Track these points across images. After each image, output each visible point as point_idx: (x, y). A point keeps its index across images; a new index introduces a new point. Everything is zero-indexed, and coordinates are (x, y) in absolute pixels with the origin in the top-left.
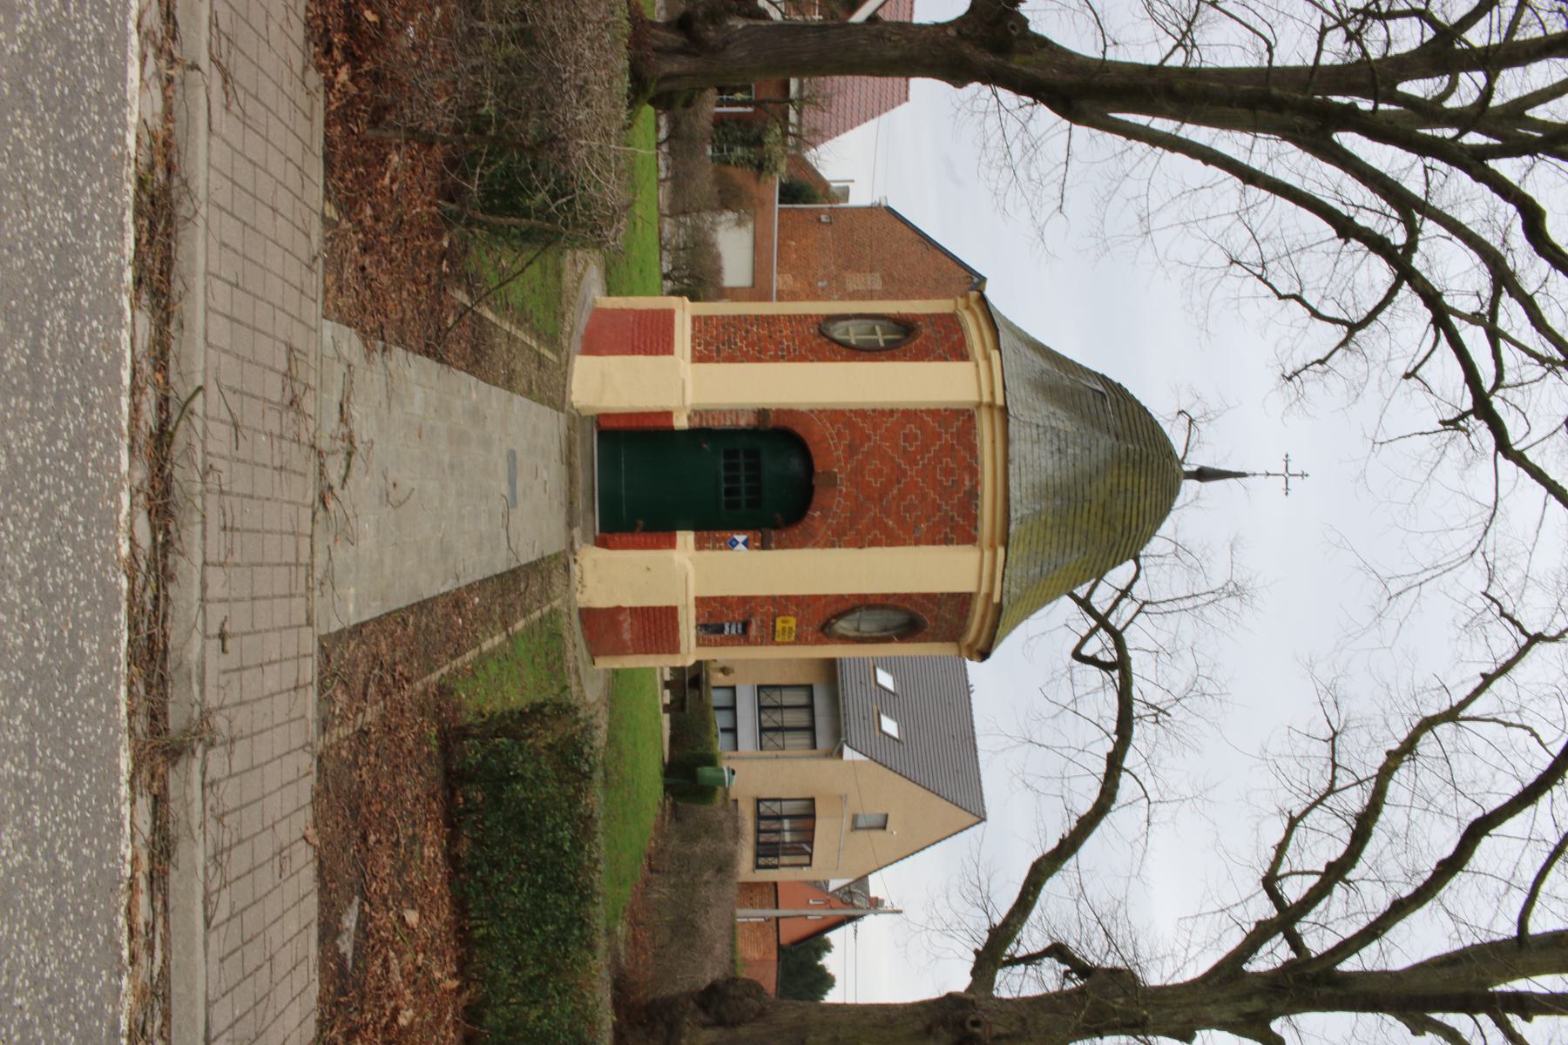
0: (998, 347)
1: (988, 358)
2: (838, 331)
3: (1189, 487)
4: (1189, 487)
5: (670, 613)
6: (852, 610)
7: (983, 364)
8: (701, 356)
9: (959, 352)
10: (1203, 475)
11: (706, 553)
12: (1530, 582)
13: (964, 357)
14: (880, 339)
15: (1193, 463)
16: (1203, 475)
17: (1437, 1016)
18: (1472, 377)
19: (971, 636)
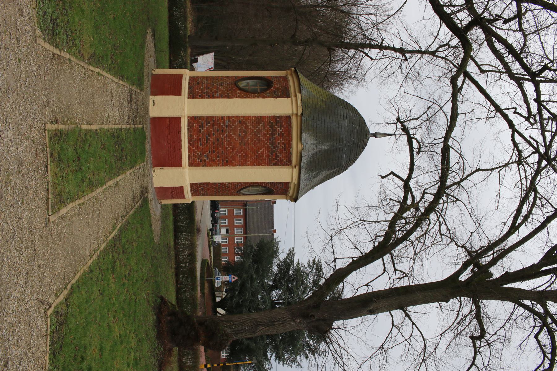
0: (300, 92)
1: (296, 96)
2: (242, 84)
3: (372, 139)
4: (372, 139)
5: (181, 188)
6: (245, 188)
7: (294, 99)
8: (192, 95)
9: (285, 94)
10: (375, 135)
11: (179, 185)
12: (360, 362)
13: (288, 96)
14: (258, 88)
15: (372, 131)
16: (375, 135)
17: (517, 224)
18: (495, 71)
19: (291, 193)
